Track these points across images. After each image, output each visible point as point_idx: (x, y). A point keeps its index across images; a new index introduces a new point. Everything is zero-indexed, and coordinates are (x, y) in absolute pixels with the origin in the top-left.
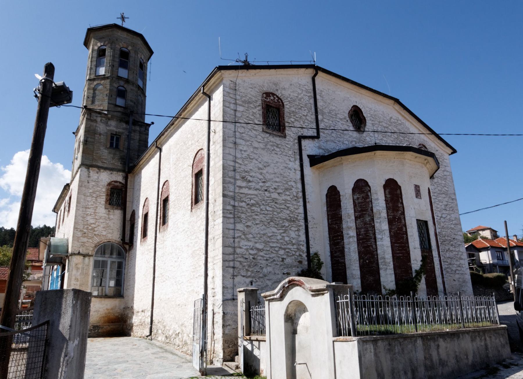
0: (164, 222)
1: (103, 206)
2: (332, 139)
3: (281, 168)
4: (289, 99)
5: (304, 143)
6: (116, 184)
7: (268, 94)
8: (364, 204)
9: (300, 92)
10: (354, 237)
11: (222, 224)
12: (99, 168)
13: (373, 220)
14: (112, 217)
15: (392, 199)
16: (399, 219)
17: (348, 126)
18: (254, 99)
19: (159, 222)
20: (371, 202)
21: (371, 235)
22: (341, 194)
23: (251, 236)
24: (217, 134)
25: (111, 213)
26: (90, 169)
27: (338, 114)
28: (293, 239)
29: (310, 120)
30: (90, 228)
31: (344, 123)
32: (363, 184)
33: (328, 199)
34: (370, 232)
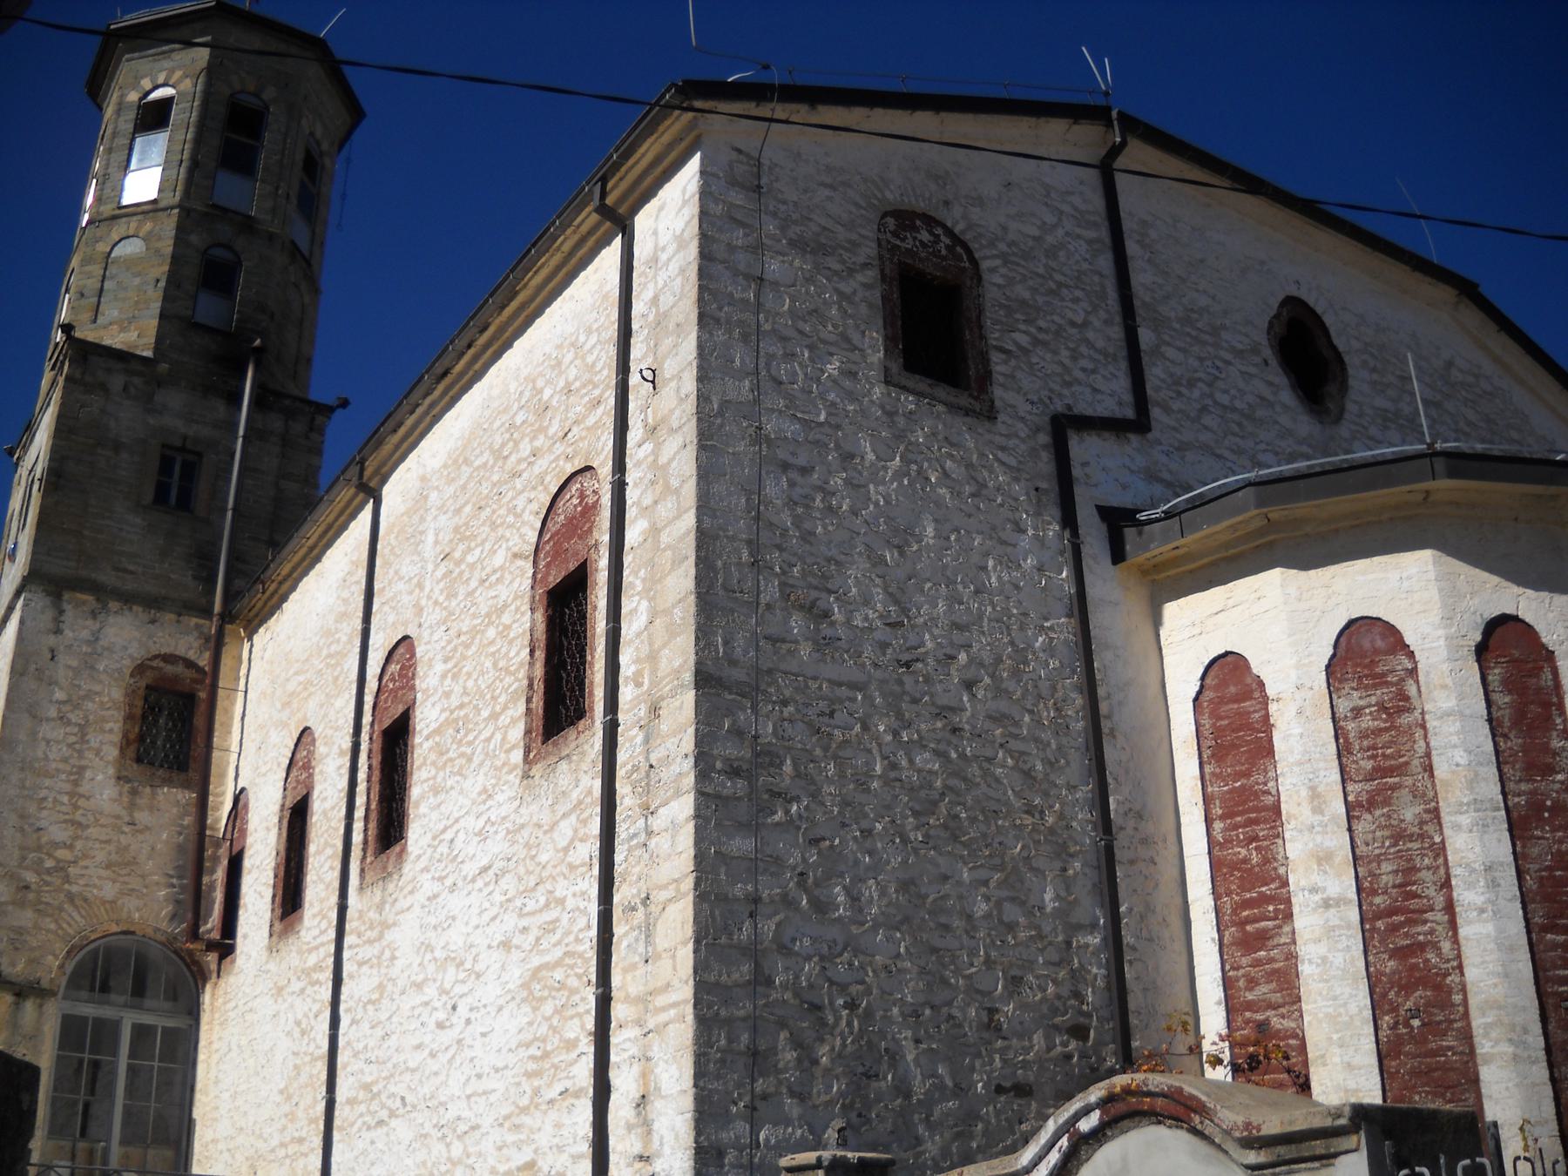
0: (390, 827)
1: (111, 771)
2: (1205, 437)
4: (1002, 247)
5: (1082, 448)
7: (905, 219)
8: (1386, 737)
9: (1050, 219)
10: (1347, 902)
11: (690, 828)
12: (102, 593)
13: (1436, 813)
15: (1520, 716)
17: (1270, 384)
18: (842, 234)
19: (357, 837)
20: (1423, 727)
21: (1431, 892)
22: (1271, 691)
24: (668, 393)
26: (66, 596)
27: (1224, 327)
29: (1100, 344)
30: (49, 864)
31: (1253, 370)
32: (1380, 643)
33: (1206, 722)
34: (1424, 874)
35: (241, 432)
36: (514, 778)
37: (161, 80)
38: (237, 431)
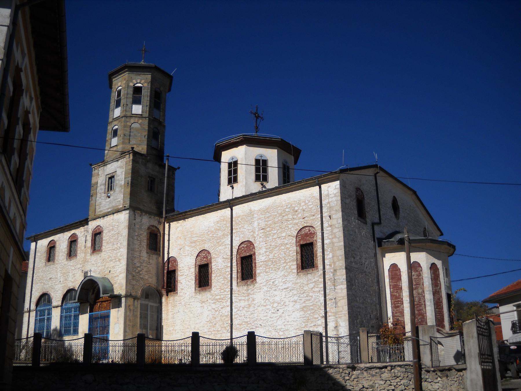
13: (424, 291)
14: (151, 261)
16: (438, 292)
19: (234, 275)
35: (166, 176)
37: (139, 82)
38: (165, 175)
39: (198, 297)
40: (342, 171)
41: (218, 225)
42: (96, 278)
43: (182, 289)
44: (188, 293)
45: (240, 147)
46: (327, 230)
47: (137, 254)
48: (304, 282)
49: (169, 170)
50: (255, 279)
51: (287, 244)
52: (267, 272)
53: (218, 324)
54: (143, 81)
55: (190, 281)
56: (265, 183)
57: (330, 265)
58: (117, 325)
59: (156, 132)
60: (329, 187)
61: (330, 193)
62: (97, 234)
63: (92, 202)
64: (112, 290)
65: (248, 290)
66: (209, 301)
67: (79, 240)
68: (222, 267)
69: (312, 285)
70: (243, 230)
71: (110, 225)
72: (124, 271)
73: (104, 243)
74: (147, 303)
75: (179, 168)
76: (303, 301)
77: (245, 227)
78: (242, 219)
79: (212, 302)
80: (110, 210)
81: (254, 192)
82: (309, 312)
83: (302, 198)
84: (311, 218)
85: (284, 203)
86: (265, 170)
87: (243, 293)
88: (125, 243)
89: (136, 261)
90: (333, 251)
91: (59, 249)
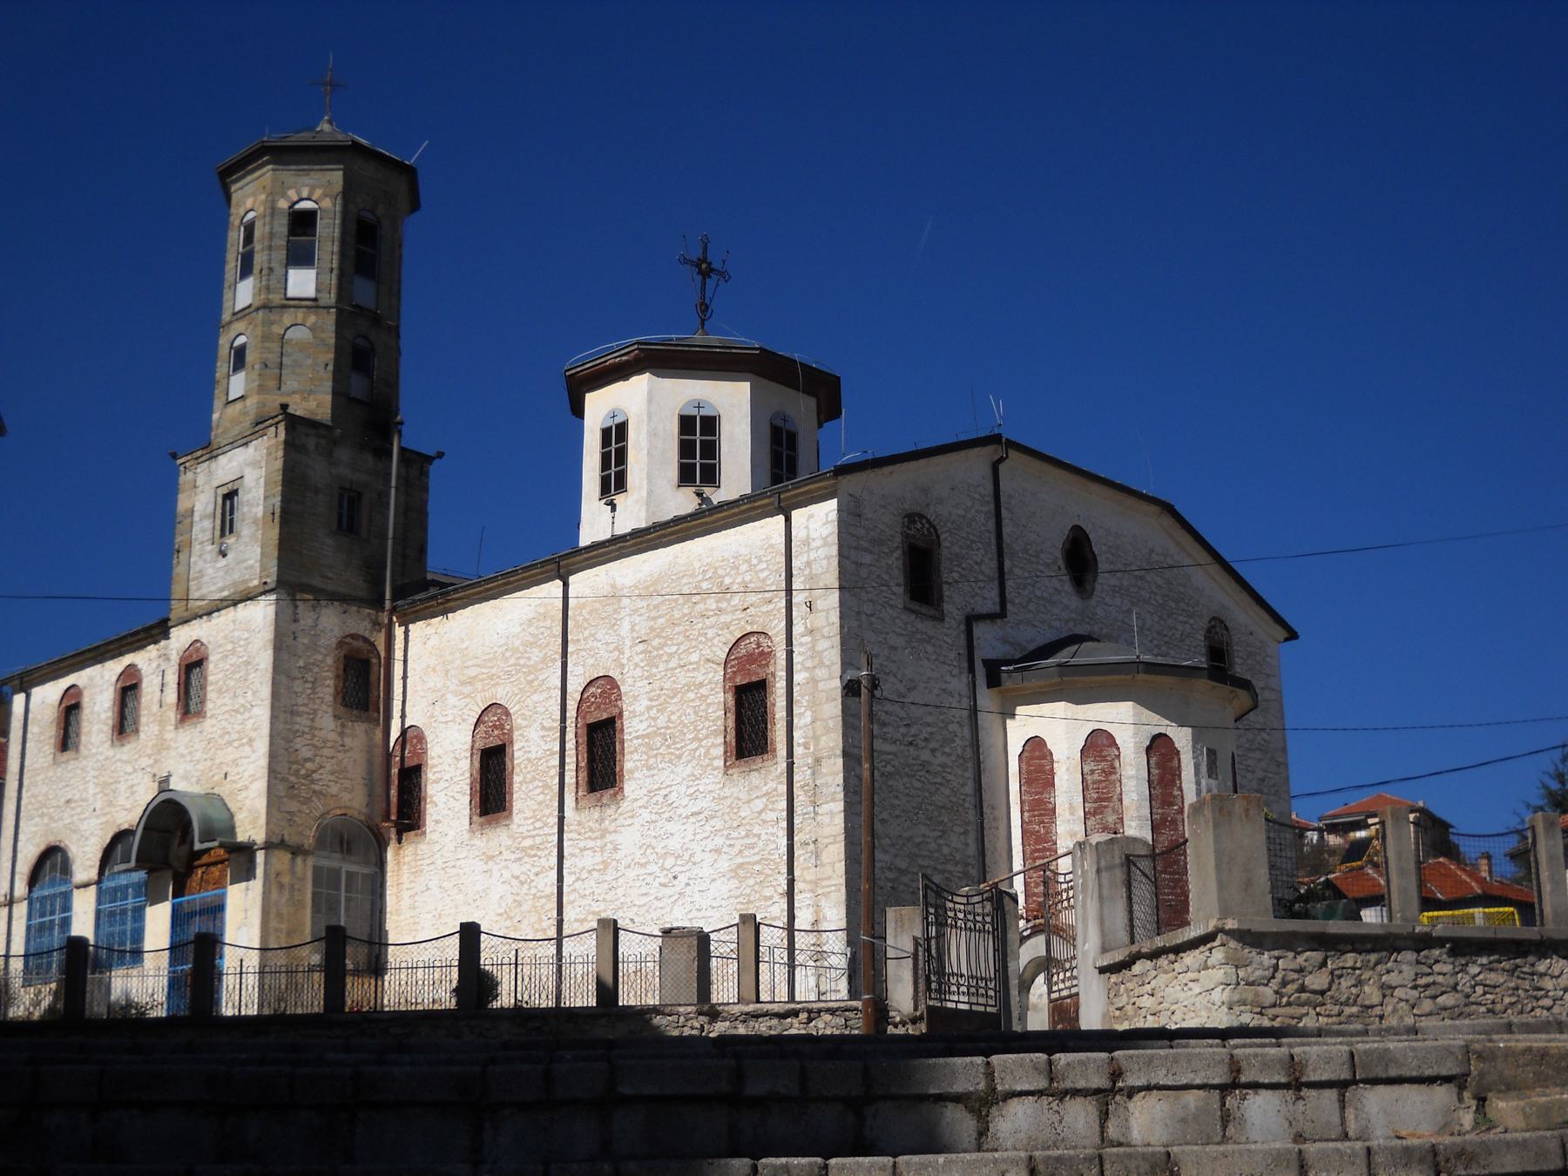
3: (936, 691)
6: (355, 643)
7: (912, 518)
14: (348, 741)
15: (1161, 780)
16: (1174, 822)
23: (887, 841)
25: (348, 731)
28: (957, 850)
36: (719, 774)
37: (305, 194)
39: (478, 843)
40: (842, 471)
41: (532, 630)
42: (184, 794)
43: (437, 822)
44: (451, 833)
45: (635, 379)
46: (801, 644)
47: (302, 722)
48: (742, 796)
49: (402, 459)
50: (622, 789)
51: (701, 685)
52: (649, 769)
53: (525, 922)
54: (318, 193)
55: (458, 796)
56: (707, 491)
57: (806, 746)
58: (244, 929)
59: (365, 346)
60: (811, 516)
61: (813, 535)
62: (193, 666)
63: (179, 570)
64: (232, 830)
65: (603, 820)
66: (506, 855)
67: (144, 685)
68: (538, 755)
69: (759, 804)
70: (596, 644)
71: (225, 637)
72: (263, 773)
73: (211, 694)
74: (335, 864)
75: (440, 455)
76: (736, 850)
77: (599, 636)
78: (590, 613)
79: (513, 857)
80: (226, 593)
81: (682, 512)
82: (751, 882)
83: (744, 551)
84: (764, 609)
85: (697, 565)
86: (711, 450)
87: (591, 830)
88: (266, 691)
89: (299, 743)
90: (814, 705)
91: (92, 712)
